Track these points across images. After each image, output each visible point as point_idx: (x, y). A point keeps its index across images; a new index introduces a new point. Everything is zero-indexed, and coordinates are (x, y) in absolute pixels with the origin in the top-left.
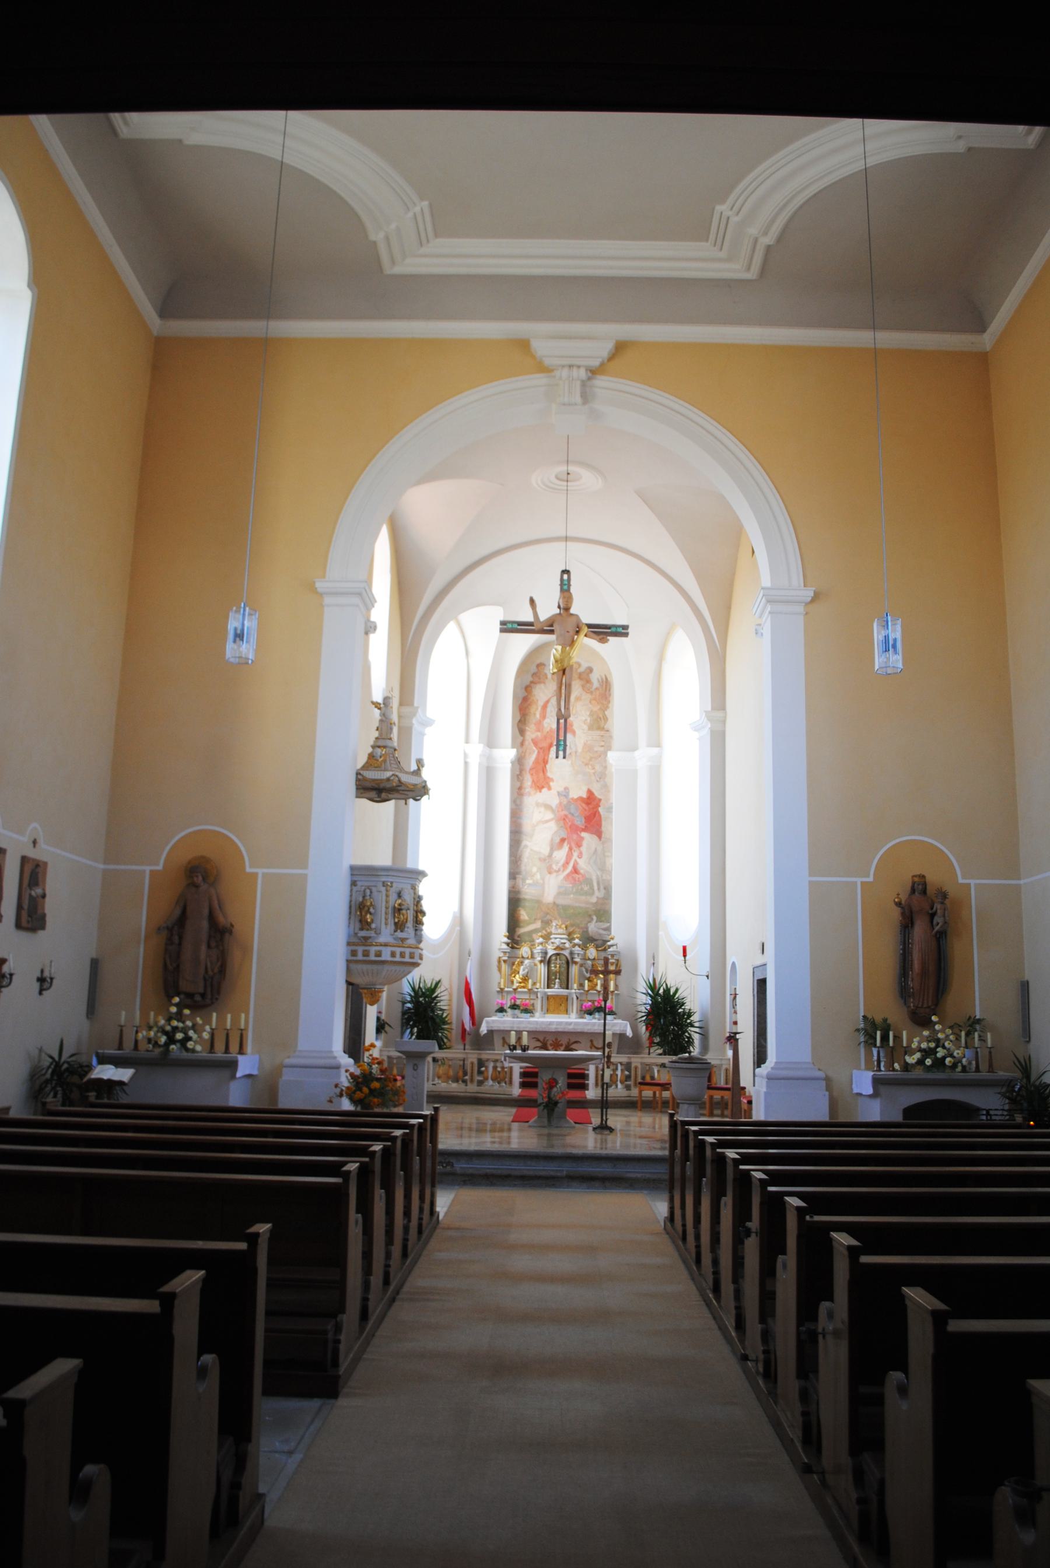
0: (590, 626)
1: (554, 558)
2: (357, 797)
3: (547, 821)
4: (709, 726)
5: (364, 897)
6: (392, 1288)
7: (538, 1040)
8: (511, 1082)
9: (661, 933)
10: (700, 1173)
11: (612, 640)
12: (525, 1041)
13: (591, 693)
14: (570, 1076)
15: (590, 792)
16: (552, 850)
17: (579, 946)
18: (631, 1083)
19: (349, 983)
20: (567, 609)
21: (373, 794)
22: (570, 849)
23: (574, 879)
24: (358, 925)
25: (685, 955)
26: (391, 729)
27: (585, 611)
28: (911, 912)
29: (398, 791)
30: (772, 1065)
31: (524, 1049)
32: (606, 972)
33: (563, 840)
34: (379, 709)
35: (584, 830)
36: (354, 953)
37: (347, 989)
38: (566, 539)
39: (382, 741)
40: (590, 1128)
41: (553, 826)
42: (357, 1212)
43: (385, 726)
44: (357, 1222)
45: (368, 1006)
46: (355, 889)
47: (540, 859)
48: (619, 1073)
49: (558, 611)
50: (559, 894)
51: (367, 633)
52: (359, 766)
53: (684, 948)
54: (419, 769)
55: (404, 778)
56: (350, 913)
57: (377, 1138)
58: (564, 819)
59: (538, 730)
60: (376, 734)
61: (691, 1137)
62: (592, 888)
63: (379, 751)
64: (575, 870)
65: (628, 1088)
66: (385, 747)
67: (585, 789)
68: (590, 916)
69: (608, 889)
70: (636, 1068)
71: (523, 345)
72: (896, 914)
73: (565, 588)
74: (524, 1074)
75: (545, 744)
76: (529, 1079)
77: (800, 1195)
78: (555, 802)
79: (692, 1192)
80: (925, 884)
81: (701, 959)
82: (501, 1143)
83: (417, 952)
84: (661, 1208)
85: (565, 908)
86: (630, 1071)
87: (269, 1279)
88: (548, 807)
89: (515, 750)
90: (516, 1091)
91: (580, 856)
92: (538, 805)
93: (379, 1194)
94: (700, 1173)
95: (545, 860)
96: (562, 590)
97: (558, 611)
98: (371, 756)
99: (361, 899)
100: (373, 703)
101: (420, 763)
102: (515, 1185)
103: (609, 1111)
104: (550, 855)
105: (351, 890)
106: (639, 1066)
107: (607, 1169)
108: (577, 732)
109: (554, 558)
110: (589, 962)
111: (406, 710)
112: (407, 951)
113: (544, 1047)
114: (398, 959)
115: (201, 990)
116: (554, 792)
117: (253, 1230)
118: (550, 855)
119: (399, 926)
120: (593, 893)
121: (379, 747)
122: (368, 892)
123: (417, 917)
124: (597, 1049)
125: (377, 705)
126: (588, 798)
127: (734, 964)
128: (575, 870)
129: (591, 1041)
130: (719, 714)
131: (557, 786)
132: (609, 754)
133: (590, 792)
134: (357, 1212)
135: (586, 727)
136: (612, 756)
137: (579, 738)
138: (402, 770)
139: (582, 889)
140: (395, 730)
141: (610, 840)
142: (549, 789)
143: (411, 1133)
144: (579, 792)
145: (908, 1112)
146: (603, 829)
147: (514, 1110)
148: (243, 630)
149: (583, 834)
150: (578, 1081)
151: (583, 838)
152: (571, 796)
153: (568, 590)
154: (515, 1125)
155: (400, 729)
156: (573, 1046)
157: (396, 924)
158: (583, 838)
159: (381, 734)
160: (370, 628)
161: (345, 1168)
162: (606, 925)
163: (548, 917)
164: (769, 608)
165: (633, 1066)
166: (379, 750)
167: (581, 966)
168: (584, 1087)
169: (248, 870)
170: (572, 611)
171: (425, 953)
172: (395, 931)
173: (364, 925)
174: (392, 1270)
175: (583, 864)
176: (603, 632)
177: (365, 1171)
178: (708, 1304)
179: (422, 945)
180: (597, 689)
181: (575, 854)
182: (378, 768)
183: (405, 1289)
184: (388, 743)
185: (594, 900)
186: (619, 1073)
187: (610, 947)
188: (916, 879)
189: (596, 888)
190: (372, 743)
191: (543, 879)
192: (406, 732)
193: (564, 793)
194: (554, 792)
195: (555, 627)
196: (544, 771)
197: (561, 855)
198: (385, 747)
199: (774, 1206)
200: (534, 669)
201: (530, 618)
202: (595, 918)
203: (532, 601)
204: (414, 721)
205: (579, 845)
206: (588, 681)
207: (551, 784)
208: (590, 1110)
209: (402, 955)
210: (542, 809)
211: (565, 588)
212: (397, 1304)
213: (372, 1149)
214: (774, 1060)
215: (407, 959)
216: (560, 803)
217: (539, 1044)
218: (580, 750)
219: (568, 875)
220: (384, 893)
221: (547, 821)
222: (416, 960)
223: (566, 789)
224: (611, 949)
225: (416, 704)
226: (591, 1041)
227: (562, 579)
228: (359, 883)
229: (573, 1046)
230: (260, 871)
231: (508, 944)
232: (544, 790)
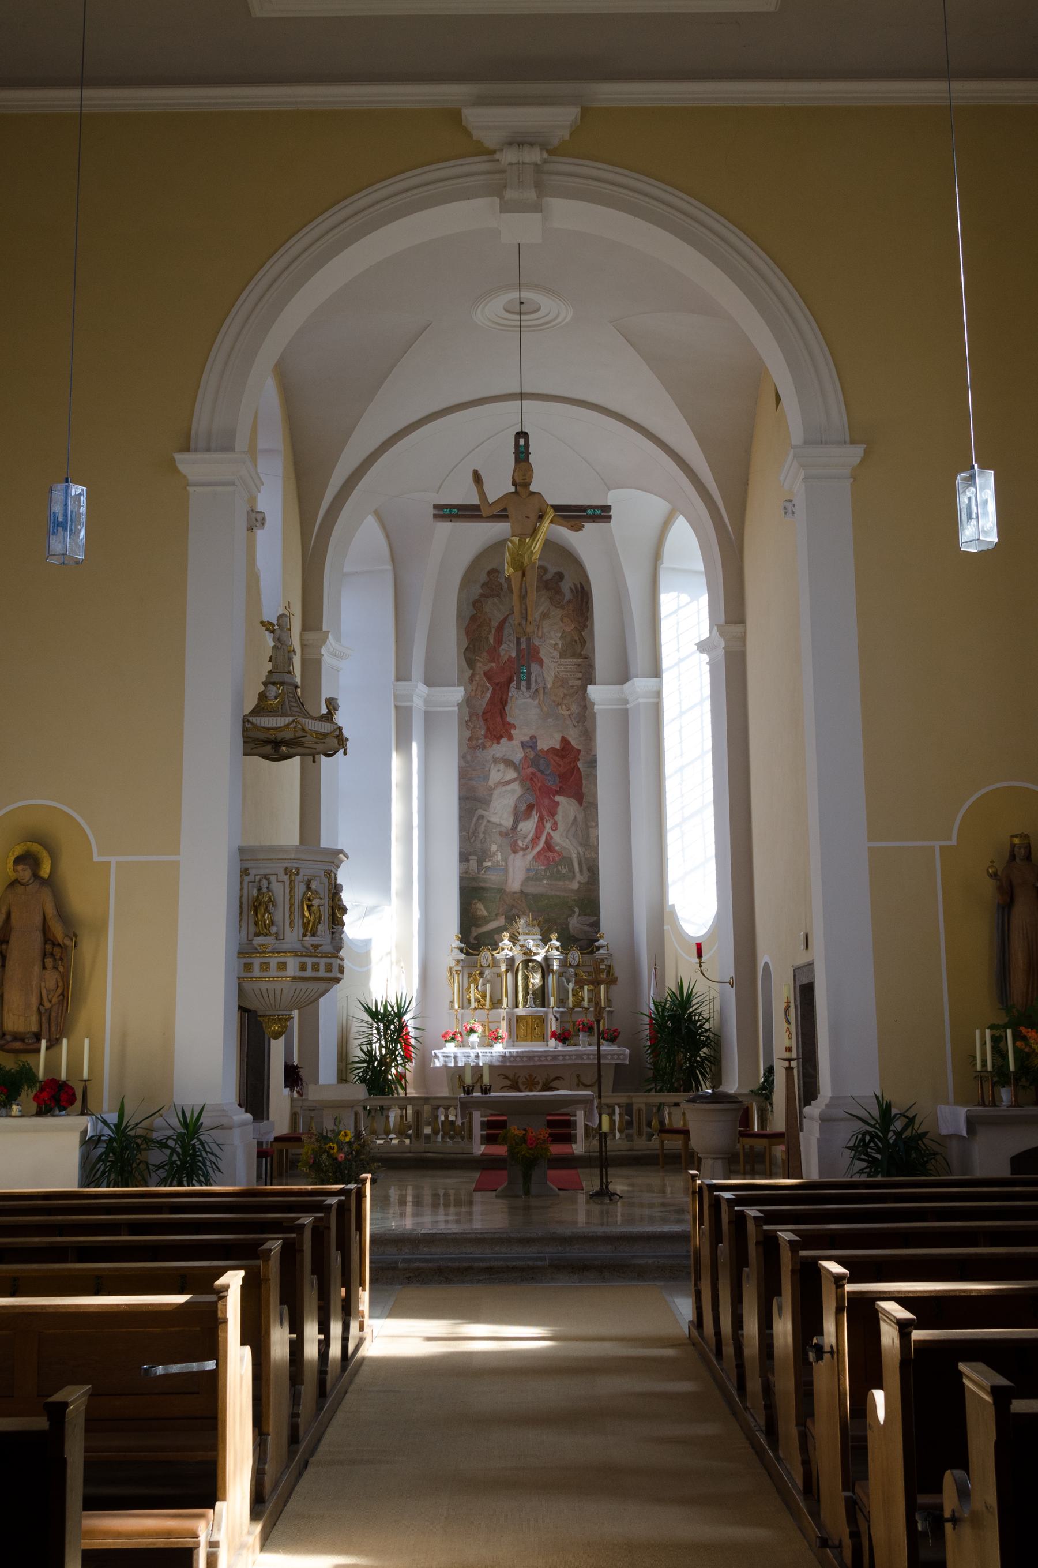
0: (557, 508)
1: (506, 417)
2: (245, 754)
3: (508, 783)
4: (723, 644)
5: (259, 890)
6: (302, 1447)
7: (506, 1077)
8: (471, 1136)
9: (666, 928)
10: (740, 1260)
11: (589, 526)
12: (486, 1080)
13: (562, 607)
14: (551, 1124)
15: (564, 741)
16: (516, 821)
17: (557, 949)
18: (634, 1131)
19: (242, 1009)
20: (527, 485)
21: (268, 749)
22: (541, 819)
23: (548, 859)
24: (252, 929)
25: (700, 955)
26: (290, 659)
27: (553, 485)
28: (1011, 885)
29: (301, 744)
30: (827, 1101)
31: (485, 1090)
32: (597, 983)
33: (530, 807)
34: (273, 632)
35: (558, 793)
36: (248, 967)
37: (242, 1018)
38: (521, 396)
39: (278, 675)
40: (582, 1198)
41: (516, 788)
42: (313, 1273)
43: (281, 656)
44: (242, 1359)
45: (273, 1041)
46: (247, 879)
47: (500, 833)
48: (617, 1118)
49: (513, 489)
50: (528, 879)
51: (251, 529)
52: (247, 711)
53: (699, 946)
54: (330, 713)
55: (311, 725)
56: (241, 913)
57: (276, 1227)
58: (532, 778)
59: (493, 661)
60: (269, 666)
61: (724, 1208)
62: (572, 870)
63: (273, 691)
64: (549, 847)
65: (630, 1138)
66: (282, 684)
67: (558, 737)
68: (571, 908)
69: (593, 871)
70: (639, 1110)
71: (454, 116)
72: (988, 888)
73: (522, 455)
74: (487, 1125)
75: (502, 679)
76: (494, 1132)
77: (903, 1300)
78: (518, 755)
79: (728, 1282)
80: (1028, 847)
81: (722, 961)
82: (458, 1221)
83: (336, 963)
84: (684, 1307)
85: (536, 897)
86: (631, 1116)
87: (88, 1465)
88: (509, 763)
89: (462, 689)
90: (480, 1149)
91: (555, 826)
92: (495, 761)
93: (336, 1257)
94: (740, 1260)
95: (507, 834)
96: (517, 461)
97: (513, 489)
98: (262, 696)
99: (255, 893)
100: (262, 623)
101: (332, 705)
102: (479, 1281)
103: (611, 1171)
104: (514, 828)
105: (241, 883)
106: (643, 1107)
107: (604, 1252)
108: (545, 660)
109: (506, 417)
110: (571, 970)
111: (311, 636)
112: (322, 962)
113: (515, 1087)
114: (309, 973)
115: (34, 1028)
116: (516, 742)
117: (57, 1397)
118: (514, 828)
119: (310, 930)
120: (574, 877)
121: (274, 684)
122: (265, 883)
123: (333, 915)
124: (586, 1087)
125: (268, 626)
126: (563, 749)
127: (766, 964)
128: (549, 847)
129: (578, 1076)
130: (737, 629)
131: (521, 734)
132: (590, 688)
133: (564, 741)
134: (313, 1273)
135: (556, 654)
136: (595, 692)
137: (552, 667)
138: (307, 715)
139: (558, 871)
140: (297, 661)
141: (595, 805)
142: (510, 738)
143: (328, 1218)
144: (548, 741)
145: (1019, 1162)
146: (585, 790)
147: (476, 1175)
148: (65, 515)
149: (558, 798)
150: (562, 1130)
151: (557, 804)
152: (539, 748)
153: (527, 459)
154: (478, 1196)
155: (304, 662)
156: (554, 1084)
157: (305, 926)
158: (557, 804)
159: (275, 666)
160: (255, 520)
161: (264, 1247)
162: (593, 919)
163: (515, 911)
164: (802, 475)
165: (635, 1107)
166: (273, 688)
167: (561, 975)
168: (570, 1139)
169: (96, 858)
170: (532, 488)
171: (347, 964)
172: (304, 935)
173: (262, 928)
174: (301, 1421)
175: (558, 838)
176: (576, 515)
177: (319, 1232)
178: (760, 1453)
179: (341, 954)
180: (569, 602)
181: (548, 825)
182: (272, 712)
183: (323, 1447)
184: (287, 678)
185: (575, 886)
186: (617, 1118)
187: (598, 948)
188: (1016, 841)
189: (577, 869)
190: (264, 679)
191: (506, 860)
192: (313, 666)
193: (530, 744)
194: (516, 742)
195: (511, 512)
196: (502, 714)
197: (528, 827)
198: (282, 684)
199: (770, 1243)
200: (483, 577)
201: (476, 501)
202: (577, 910)
203: (477, 478)
204: (323, 651)
205: (553, 814)
206: (558, 592)
207: (512, 732)
208: (579, 1170)
209: (316, 967)
210: (502, 767)
211: (522, 455)
212: (310, 1470)
213: (300, 1221)
214: (829, 1094)
215: (322, 973)
216: (526, 757)
217: (508, 1083)
218: (549, 686)
219: (539, 853)
220: (287, 883)
221: (508, 783)
222: (335, 974)
223: (533, 738)
224: (601, 951)
225: (325, 628)
226: (578, 1076)
227: (517, 445)
228: (253, 872)
229: (554, 1084)
230: (113, 860)
231: (461, 950)
232: (504, 741)
